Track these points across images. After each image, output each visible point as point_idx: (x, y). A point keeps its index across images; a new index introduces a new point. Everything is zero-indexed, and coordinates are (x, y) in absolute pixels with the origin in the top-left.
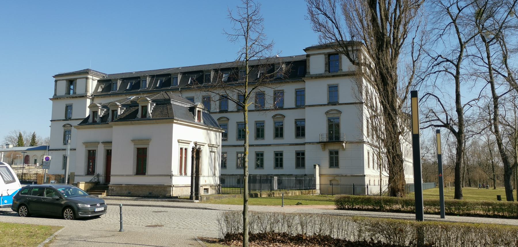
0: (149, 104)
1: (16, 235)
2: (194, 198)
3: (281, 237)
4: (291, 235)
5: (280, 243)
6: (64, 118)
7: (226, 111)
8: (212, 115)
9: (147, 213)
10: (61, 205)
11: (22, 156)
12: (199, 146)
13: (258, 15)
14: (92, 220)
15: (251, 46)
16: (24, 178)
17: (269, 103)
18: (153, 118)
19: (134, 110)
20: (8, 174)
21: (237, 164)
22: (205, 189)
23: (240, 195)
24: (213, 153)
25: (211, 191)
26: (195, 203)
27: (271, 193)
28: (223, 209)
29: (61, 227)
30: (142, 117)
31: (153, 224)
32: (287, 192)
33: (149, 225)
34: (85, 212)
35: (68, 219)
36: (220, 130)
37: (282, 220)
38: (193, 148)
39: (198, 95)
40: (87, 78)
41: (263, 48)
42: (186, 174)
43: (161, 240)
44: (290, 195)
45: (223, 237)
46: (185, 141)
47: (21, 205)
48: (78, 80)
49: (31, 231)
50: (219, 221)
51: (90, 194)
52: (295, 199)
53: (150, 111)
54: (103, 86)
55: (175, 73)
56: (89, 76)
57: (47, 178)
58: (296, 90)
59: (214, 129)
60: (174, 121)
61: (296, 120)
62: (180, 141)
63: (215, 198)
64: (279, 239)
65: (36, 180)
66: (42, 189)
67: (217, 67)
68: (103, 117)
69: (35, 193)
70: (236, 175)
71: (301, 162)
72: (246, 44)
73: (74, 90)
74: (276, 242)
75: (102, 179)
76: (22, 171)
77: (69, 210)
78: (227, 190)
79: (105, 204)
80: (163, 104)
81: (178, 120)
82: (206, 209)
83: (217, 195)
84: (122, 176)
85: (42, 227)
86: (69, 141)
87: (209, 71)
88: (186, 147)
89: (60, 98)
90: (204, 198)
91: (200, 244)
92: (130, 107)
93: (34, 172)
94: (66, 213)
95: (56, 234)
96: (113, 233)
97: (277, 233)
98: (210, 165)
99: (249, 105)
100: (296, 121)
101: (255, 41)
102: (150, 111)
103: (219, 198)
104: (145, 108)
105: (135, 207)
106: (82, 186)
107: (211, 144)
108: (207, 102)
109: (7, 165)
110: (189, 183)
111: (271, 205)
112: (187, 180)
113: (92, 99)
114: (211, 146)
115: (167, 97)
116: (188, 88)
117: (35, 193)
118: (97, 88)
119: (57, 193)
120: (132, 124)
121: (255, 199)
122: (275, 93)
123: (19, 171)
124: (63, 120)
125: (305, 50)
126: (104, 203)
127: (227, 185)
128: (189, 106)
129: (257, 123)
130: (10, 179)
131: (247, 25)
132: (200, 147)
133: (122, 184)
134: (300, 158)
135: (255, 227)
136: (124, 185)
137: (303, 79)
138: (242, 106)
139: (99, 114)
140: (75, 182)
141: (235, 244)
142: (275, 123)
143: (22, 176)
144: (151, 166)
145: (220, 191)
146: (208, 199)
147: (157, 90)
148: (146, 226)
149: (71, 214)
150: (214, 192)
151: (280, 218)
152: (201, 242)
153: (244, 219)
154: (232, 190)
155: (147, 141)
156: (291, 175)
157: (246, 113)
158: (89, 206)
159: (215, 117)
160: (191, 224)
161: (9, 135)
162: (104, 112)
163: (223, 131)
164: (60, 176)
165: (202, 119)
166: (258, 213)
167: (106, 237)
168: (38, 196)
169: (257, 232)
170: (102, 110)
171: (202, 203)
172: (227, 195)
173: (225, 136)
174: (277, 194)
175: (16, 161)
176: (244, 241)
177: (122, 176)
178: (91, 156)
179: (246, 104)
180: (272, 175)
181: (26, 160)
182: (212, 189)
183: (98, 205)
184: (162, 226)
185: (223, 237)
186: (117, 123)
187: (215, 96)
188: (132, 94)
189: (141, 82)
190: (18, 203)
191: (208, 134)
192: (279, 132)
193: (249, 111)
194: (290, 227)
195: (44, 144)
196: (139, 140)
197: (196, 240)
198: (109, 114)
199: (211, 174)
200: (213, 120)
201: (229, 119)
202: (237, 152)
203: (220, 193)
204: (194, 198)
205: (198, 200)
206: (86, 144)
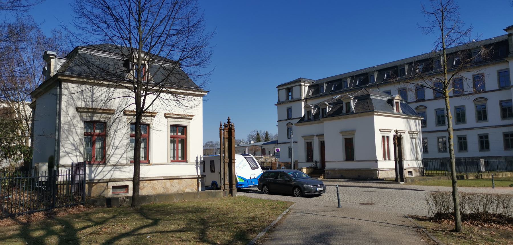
0: (352, 100)
1: (263, 207)
2: (399, 180)
3: (497, 218)
4: (508, 217)
5: (496, 223)
6: (286, 118)
7: (424, 100)
8: (410, 105)
9: (359, 192)
10: (291, 185)
11: (260, 149)
12: (400, 134)
13: (453, 4)
14: (315, 198)
15: (447, 35)
16: (263, 165)
17: (468, 86)
18: (356, 112)
19: (339, 107)
20: (253, 162)
21: (439, 148)
22: (409, 172)
23: (445, 177)
24: (414, 139)
25: (415, 173)
26: (401, 184)
27: (479, 175)
28: (429, 190)
29: (294, 203)
30: (347, 112)
31: (365, 202)
32: (497, 173)
33: (362, 202)
34: (309, 191)
35: (297, 196)
36: (419, 118)
37: (496, 201)
38: (394, 136)
39: (394, 88)
40: (300, 85)
41: (460, 35)
42: (389, 159)
43: (374, 216)
44: (500, 176)
45: (433, 216)
46: (388, 130)
47: (264, 185)
48: (294, 88)
49: (273, 205)
50: (427, 200)
51: (311, 177)
52: (507, 181)
53: (353, 106)
54: (313, 90)
55: (372, 72)
56: (302, 84)
57: (279, 165)
58: (498, 71)
59: (413, 117)
60: (375, 113)
61: (500, 101)
62: (382, 130)
63: (420, 180)
64: (494, 220)
65: (271, 166)
66: (277, 173)
67: (410, 61)
68: (315, 114)
69: (272, 177)
70: (439, 158)
71: (510, 143)
72: (442, 33)
73: (292, 95)
74: (491, 223)
75: (319, 165)
76: (261, 160)
77: (297, 189)
78: (429, 173)
79: (324, 185)
80: (364, 99)
81: (378, 112)
82: (412, 190)
83: (422, 177)
84: (335, 162)
85: (280, 202)
86: (292, 136)
87: (403, 65)
88: (388, 135)
89: (282, 104)
90: (409, 179)
91: (411, 221)
92: (336, 104)
93: (269, 161)
94: (295, 192)
95: (290, 207)
96: (333, 209)
97: (491, 214)
98: (412, 150)
99: (449, 91)
100: (501, 102)
101: (451, 29)
102: (353, 106)
103: (424, 180)
104: (348, 105)
105: (348, 188)
106: (304, 171)
107: (411, 131)
108: (403, 93)
109: (252, 156)
110: (394, 167)
111: (480, 186)
112: (391, 164)
113: (306, 102)
114: (411, 133)
115: (366, 93)
116: (386, 83)
117: (272, 177)
118: (308, 92)
119: (288, 176)
120: (339, 119)
121: (462, 181)
122: (475, 77)
123: (259, 160)
124: (286, 120)
125: (505, 30)
126: (323, 184)
127: (430, 168)
128: (387, 98)
129: (456, 108)
130: (254, 166)
131: (441, 15)
132: (401, 134)
133: (335, 169)
134: (508, 139)
135: (466, 207)
136: (337, 170)
137: (506, 59)
138: (442, 93)
139: (312, 113)
140: (299, 168)
141: (446, 222)
142: (477, 106)
143: (262, 164)
144: (358, 153)
145: (424, 174)
146: (413, 181)
147: (357, 88)
148: (359, 204)
149: (299, 192)
150: (418, 174)
151: (493, 199)
152: (411, 219)
153: (455, 200)
154: (436, 173)
155: (353, 131)
156: (500, 157)
157: (448, 99)
158: (312, 186)
159: (413, 106)
160: (399, 203)
161: (251, 134)
162: (315, 111)
163: (422, 118)
164: (287, 163)
165: (400, 109)
166: (468, 194)
167: (328, 211)
168: (275, 178)
169: (469, 213)
170: (314, 109)
171: (407, 184)
172: (431, 177)
173: (424, 123)
174: (485, 175)
175: (256, 153)
176: (456, 220)
177: (335, 162)
178: (309, 147)
179: (447, 91)
180: (478, 157)
181: (263, 152)
182: (416, 172)
183: (319, 186)
184: (372, 204)
185: (433, 216)
186: (326, 118)
187: (411, 86)
188: (337, 94)
189: (343, 83)
190: (262, 184)
191: (408, 122)
192: (482, 115)
193: (450, 97)
194: (507, 208)
195: (274, 140)
196: (346, 132)
197: (406, 217)
198: (319, 112)
199: (413, 158)
200: (411, 109)
201: (487, 99)
202: (437, 137)
203: (424, 176)
204: (399, 180)
205: (403, 181)
206: (305, 137)
